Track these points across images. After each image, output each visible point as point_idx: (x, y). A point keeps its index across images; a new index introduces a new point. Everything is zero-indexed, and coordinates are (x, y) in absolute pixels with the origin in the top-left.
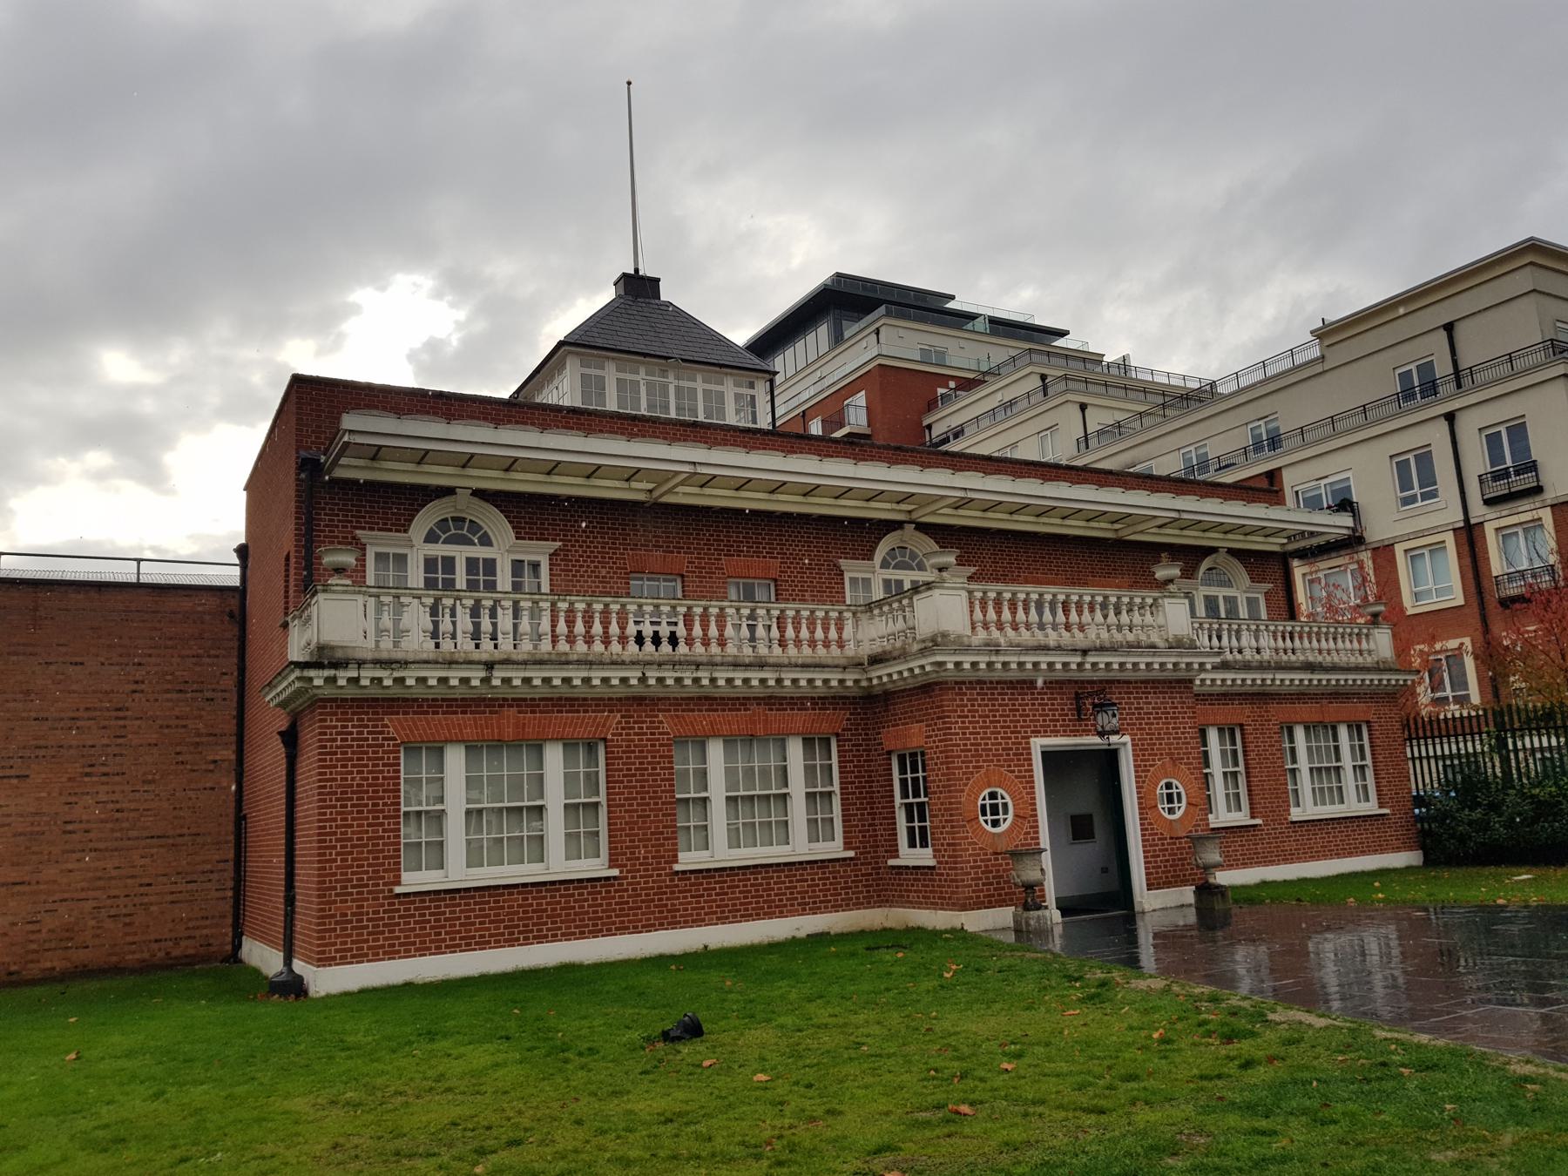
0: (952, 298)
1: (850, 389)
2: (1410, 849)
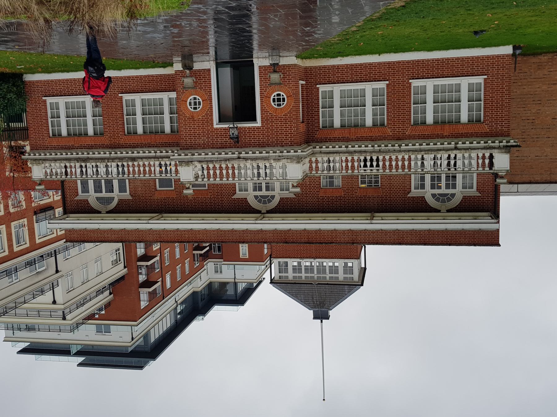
0: (80, 365)
1: (148, 309)
2: (30, 82)
